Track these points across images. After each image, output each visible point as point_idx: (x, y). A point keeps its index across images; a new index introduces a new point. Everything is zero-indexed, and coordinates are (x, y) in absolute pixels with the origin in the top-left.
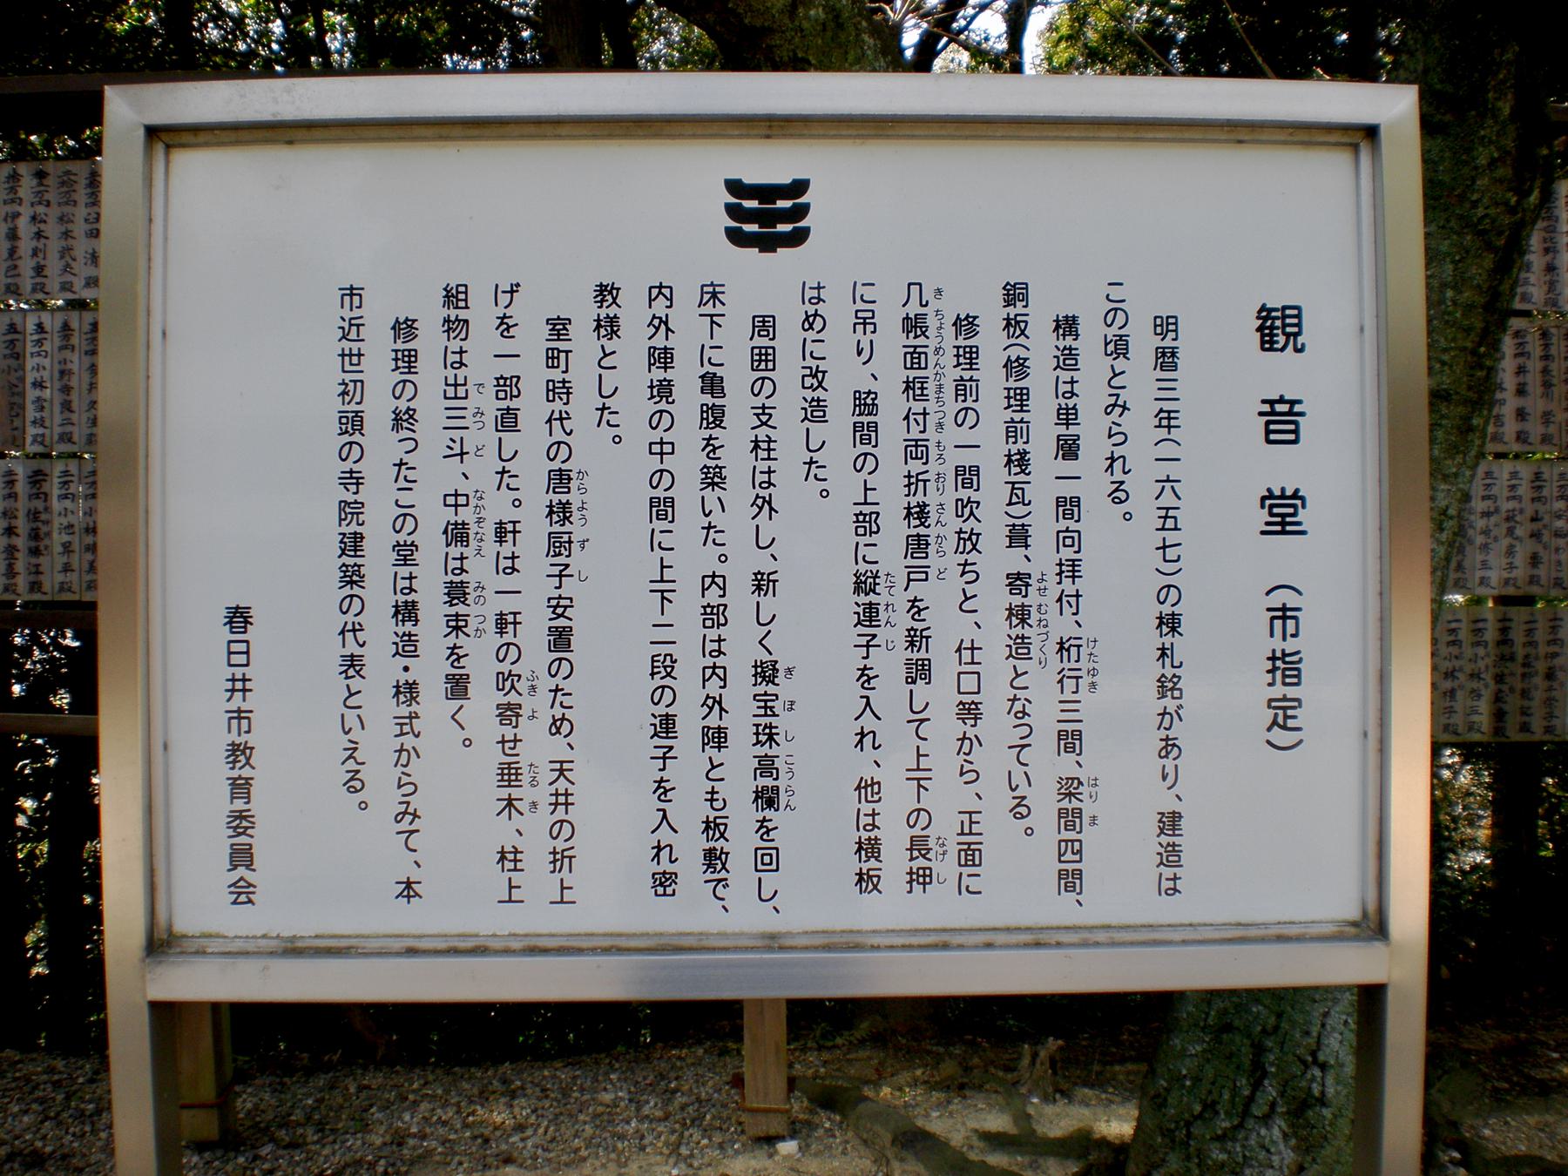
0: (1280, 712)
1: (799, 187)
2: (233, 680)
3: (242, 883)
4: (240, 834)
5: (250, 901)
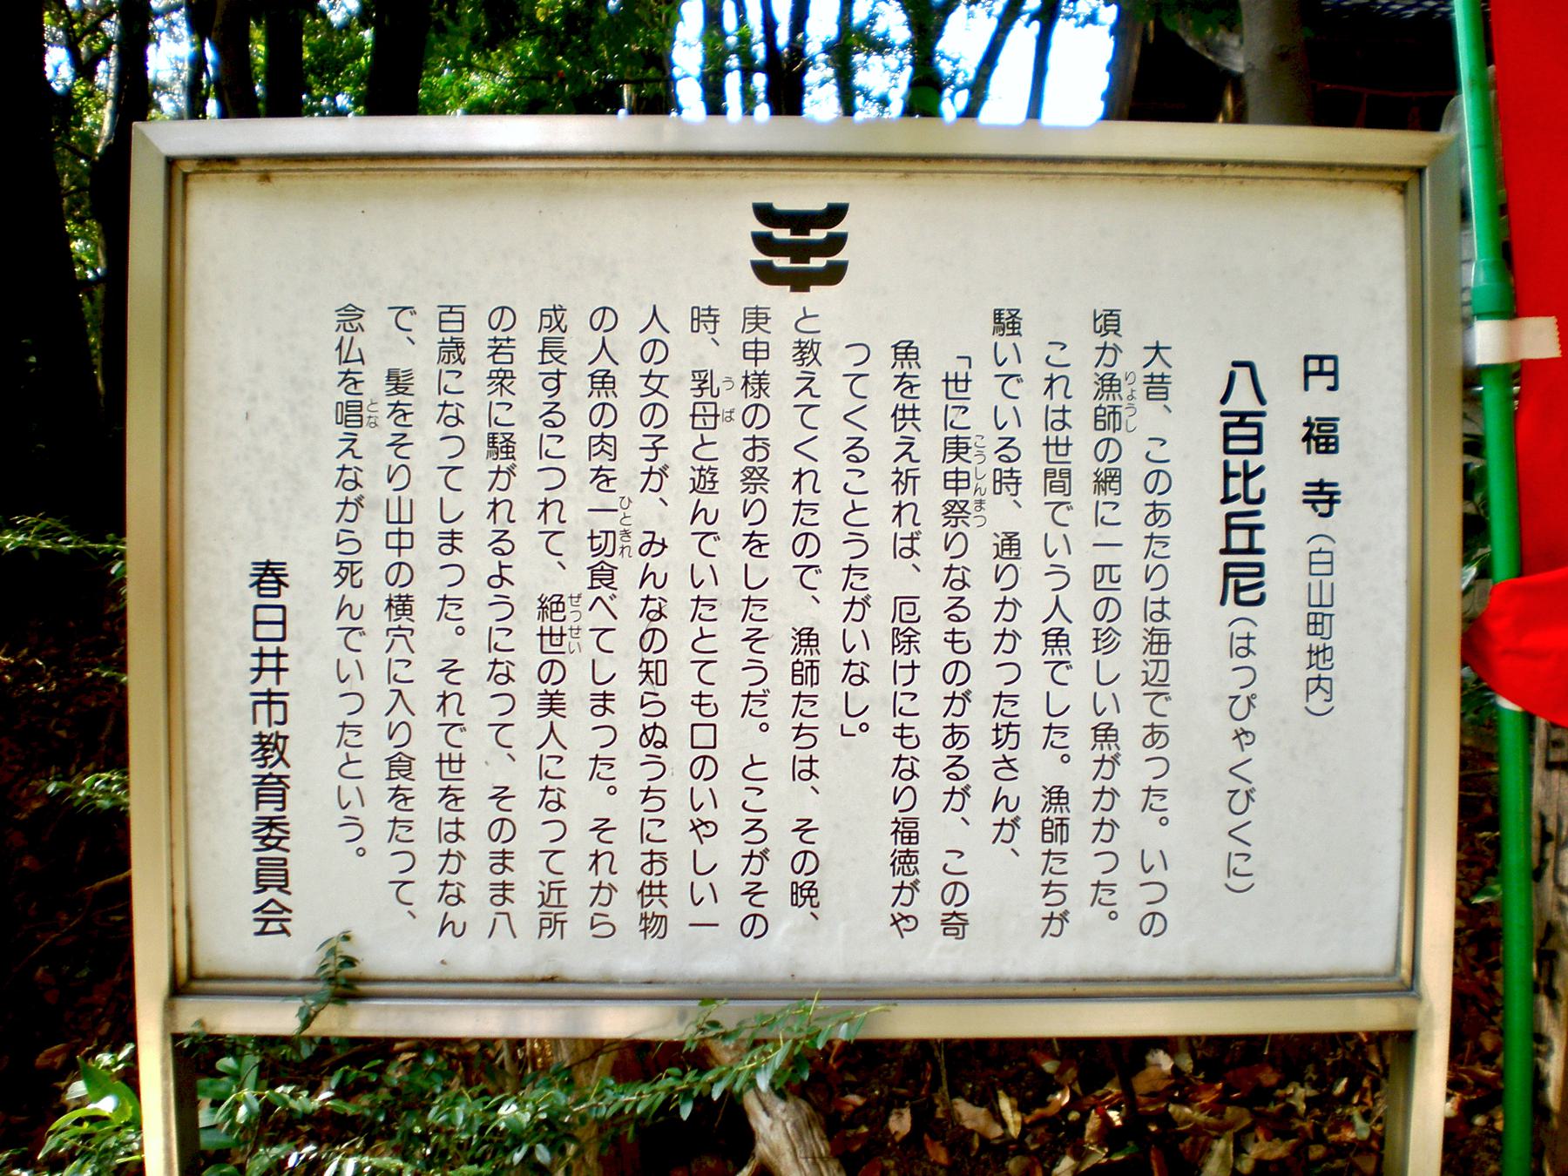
1: (836, 213)
2: (261, 655)
3: (272, 907)
4: (270, 847)
5: (284, 931)
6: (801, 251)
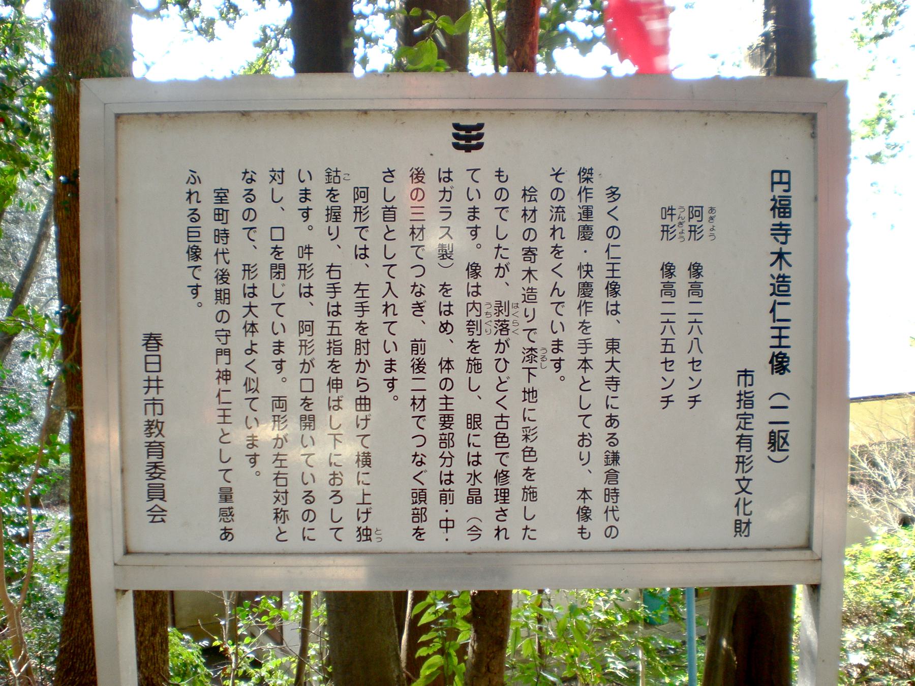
0: (743, 421)
1: (480, 126)
2: (149, 380)
3: (156, 509)
4: (155, 478)
5: (163, 521)
6: (468, 139)
